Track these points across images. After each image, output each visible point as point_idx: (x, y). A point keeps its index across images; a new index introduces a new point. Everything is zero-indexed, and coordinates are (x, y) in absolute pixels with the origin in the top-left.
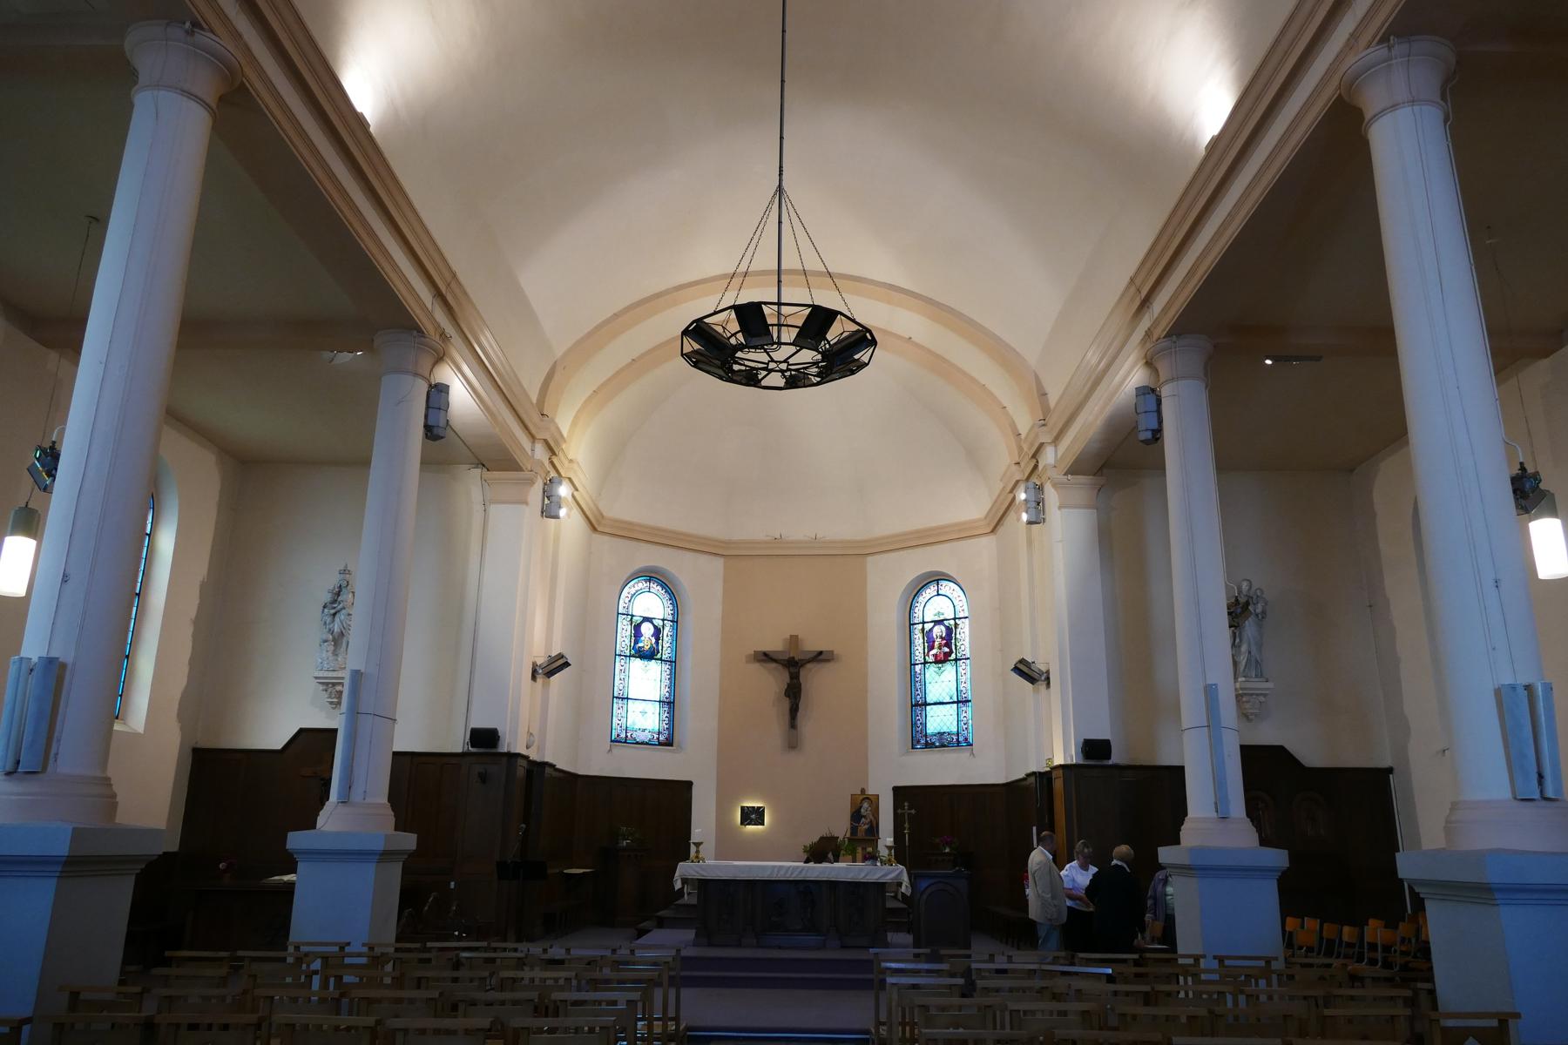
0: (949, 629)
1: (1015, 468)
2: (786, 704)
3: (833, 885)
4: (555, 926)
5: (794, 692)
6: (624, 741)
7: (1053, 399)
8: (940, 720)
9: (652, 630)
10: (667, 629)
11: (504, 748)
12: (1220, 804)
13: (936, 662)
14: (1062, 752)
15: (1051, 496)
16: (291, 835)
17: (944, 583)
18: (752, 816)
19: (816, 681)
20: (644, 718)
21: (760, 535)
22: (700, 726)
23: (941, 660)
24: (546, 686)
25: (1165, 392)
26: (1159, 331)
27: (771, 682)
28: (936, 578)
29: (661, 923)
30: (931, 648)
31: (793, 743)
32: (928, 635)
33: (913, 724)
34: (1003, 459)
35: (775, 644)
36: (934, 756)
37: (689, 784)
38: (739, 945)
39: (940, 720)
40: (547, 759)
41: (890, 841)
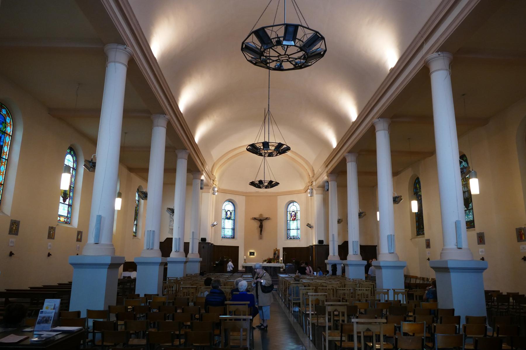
2: (259, 229)
3: (271, 267)
5: (261, 227)
7: (315, 172)
8: (293, 233)
11: (207, 242)
12: (334, 253)
14: (315, 242)
15: (315, 192)
18: (252, 254)
19: (266, 224)
20: (228, 232)
22: (240, 234)
23: (294, 220)
25: (330, 183)
26: (329, 172)
27: (256, 224)
28: (293, 202)
31: (261, 238)
33: (287, 234)
34: (307, 180)
35: (257, 216)
36: (292, 241)
39: (293, 233)
41: (282, 259)
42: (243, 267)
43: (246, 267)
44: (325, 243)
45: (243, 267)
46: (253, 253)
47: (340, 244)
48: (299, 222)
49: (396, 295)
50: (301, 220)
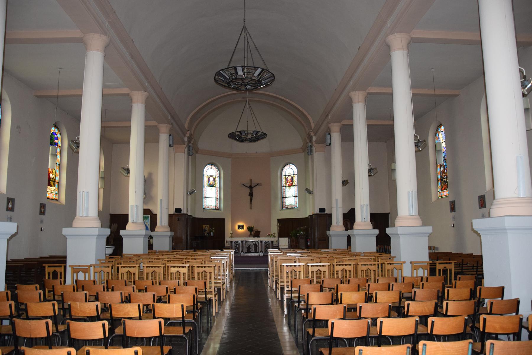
0: (292, 178)
5: (251, 195)
16: (64, 229)
31: (251, 208)
32: (287, 179)
37: (224, 219)
44: (327, 212)
46: (242, 226)
47: (346, 212)
49: (75, 275)
50: (299, 185)
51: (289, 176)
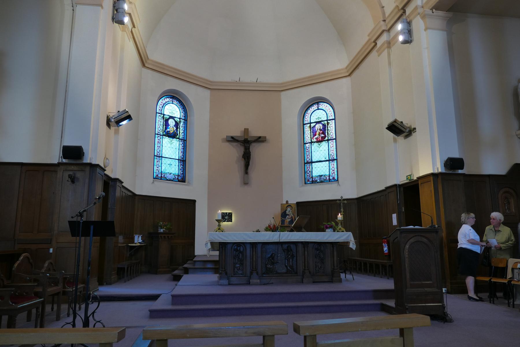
0: (324, 125)
1: (382, 23)
2: (242, 163)
4: (123, 275)
5: (247, 157)
6: (161, 178)
9: (174, 123)
10: (182, 123)
11: (87, 159)
13: (317, 142)
15: (418, 24)
17: (321, 104)
18: (227, 217)
19: (256, 150)
20: (171, 168)
21: (229, 80)
22: (199, 171)
23: (319, 141)
24: (117, 132)
27: (235, 152)
28: (317, 101)
29: (186, 271)
30: (315, 135)
31: (246, 183)
32: (312, 129)
35: (237, 133)
37: (194, 201)
38: (248, 283)
39: (319, 170)
40: (117, 177)
42: (214, 246)
43: (222, 246)
45: (214, 246)
46: (230, 215)
48: (332, 144)
51: (317, 123)
